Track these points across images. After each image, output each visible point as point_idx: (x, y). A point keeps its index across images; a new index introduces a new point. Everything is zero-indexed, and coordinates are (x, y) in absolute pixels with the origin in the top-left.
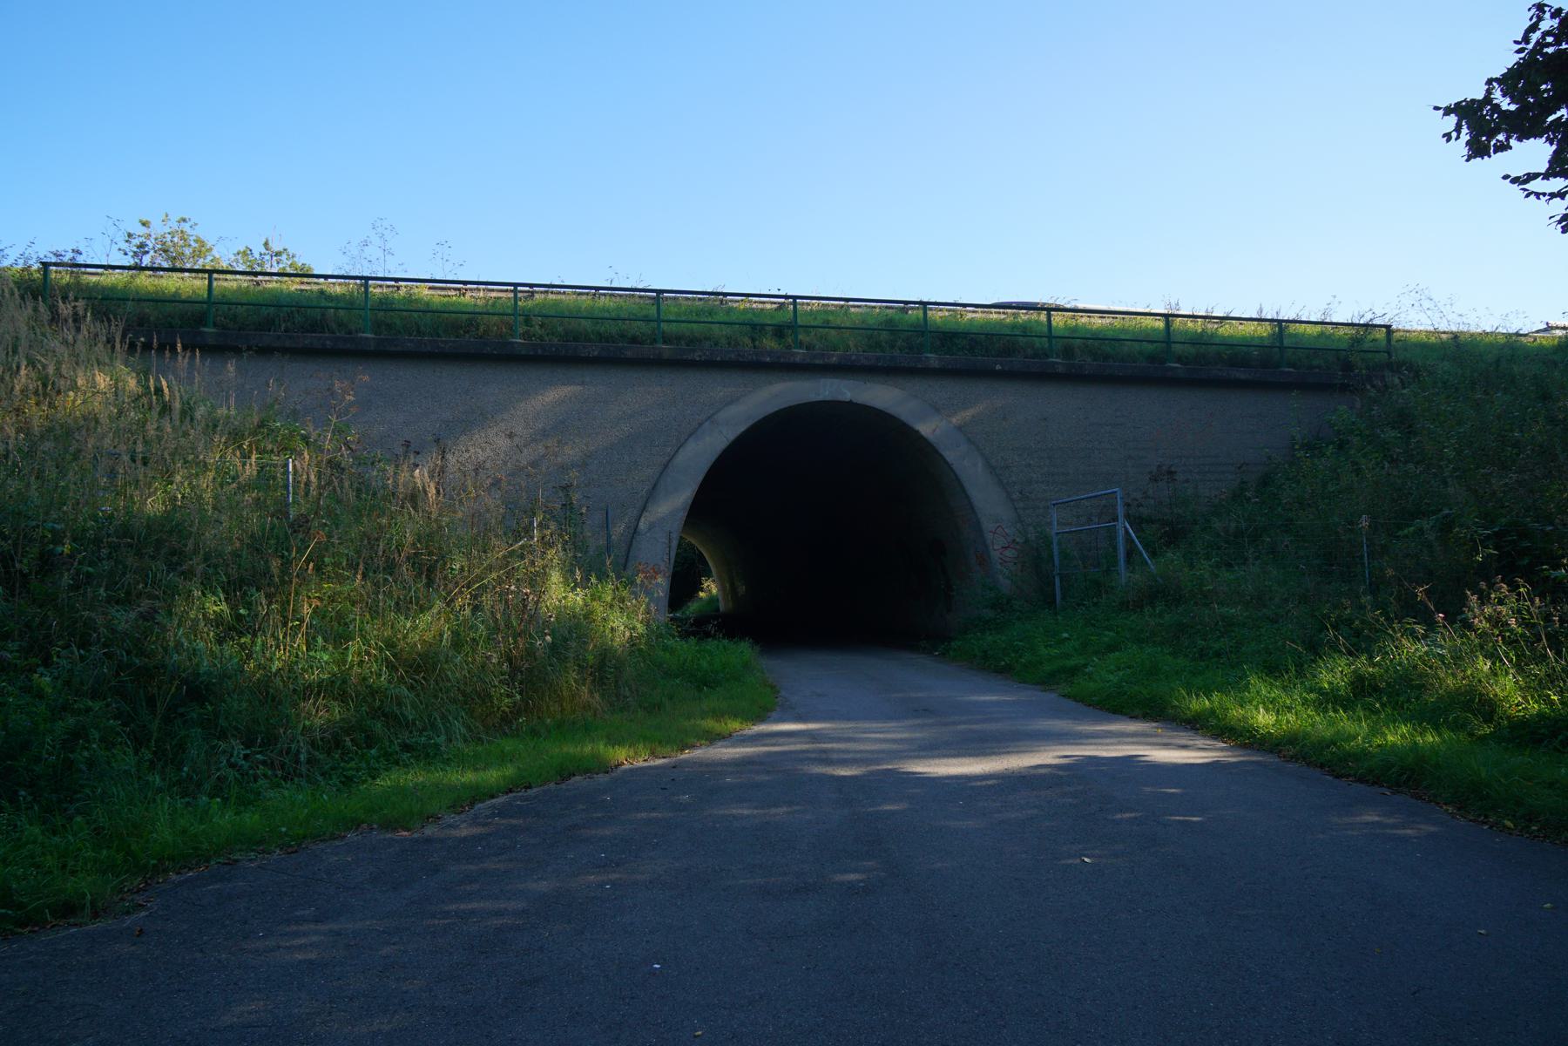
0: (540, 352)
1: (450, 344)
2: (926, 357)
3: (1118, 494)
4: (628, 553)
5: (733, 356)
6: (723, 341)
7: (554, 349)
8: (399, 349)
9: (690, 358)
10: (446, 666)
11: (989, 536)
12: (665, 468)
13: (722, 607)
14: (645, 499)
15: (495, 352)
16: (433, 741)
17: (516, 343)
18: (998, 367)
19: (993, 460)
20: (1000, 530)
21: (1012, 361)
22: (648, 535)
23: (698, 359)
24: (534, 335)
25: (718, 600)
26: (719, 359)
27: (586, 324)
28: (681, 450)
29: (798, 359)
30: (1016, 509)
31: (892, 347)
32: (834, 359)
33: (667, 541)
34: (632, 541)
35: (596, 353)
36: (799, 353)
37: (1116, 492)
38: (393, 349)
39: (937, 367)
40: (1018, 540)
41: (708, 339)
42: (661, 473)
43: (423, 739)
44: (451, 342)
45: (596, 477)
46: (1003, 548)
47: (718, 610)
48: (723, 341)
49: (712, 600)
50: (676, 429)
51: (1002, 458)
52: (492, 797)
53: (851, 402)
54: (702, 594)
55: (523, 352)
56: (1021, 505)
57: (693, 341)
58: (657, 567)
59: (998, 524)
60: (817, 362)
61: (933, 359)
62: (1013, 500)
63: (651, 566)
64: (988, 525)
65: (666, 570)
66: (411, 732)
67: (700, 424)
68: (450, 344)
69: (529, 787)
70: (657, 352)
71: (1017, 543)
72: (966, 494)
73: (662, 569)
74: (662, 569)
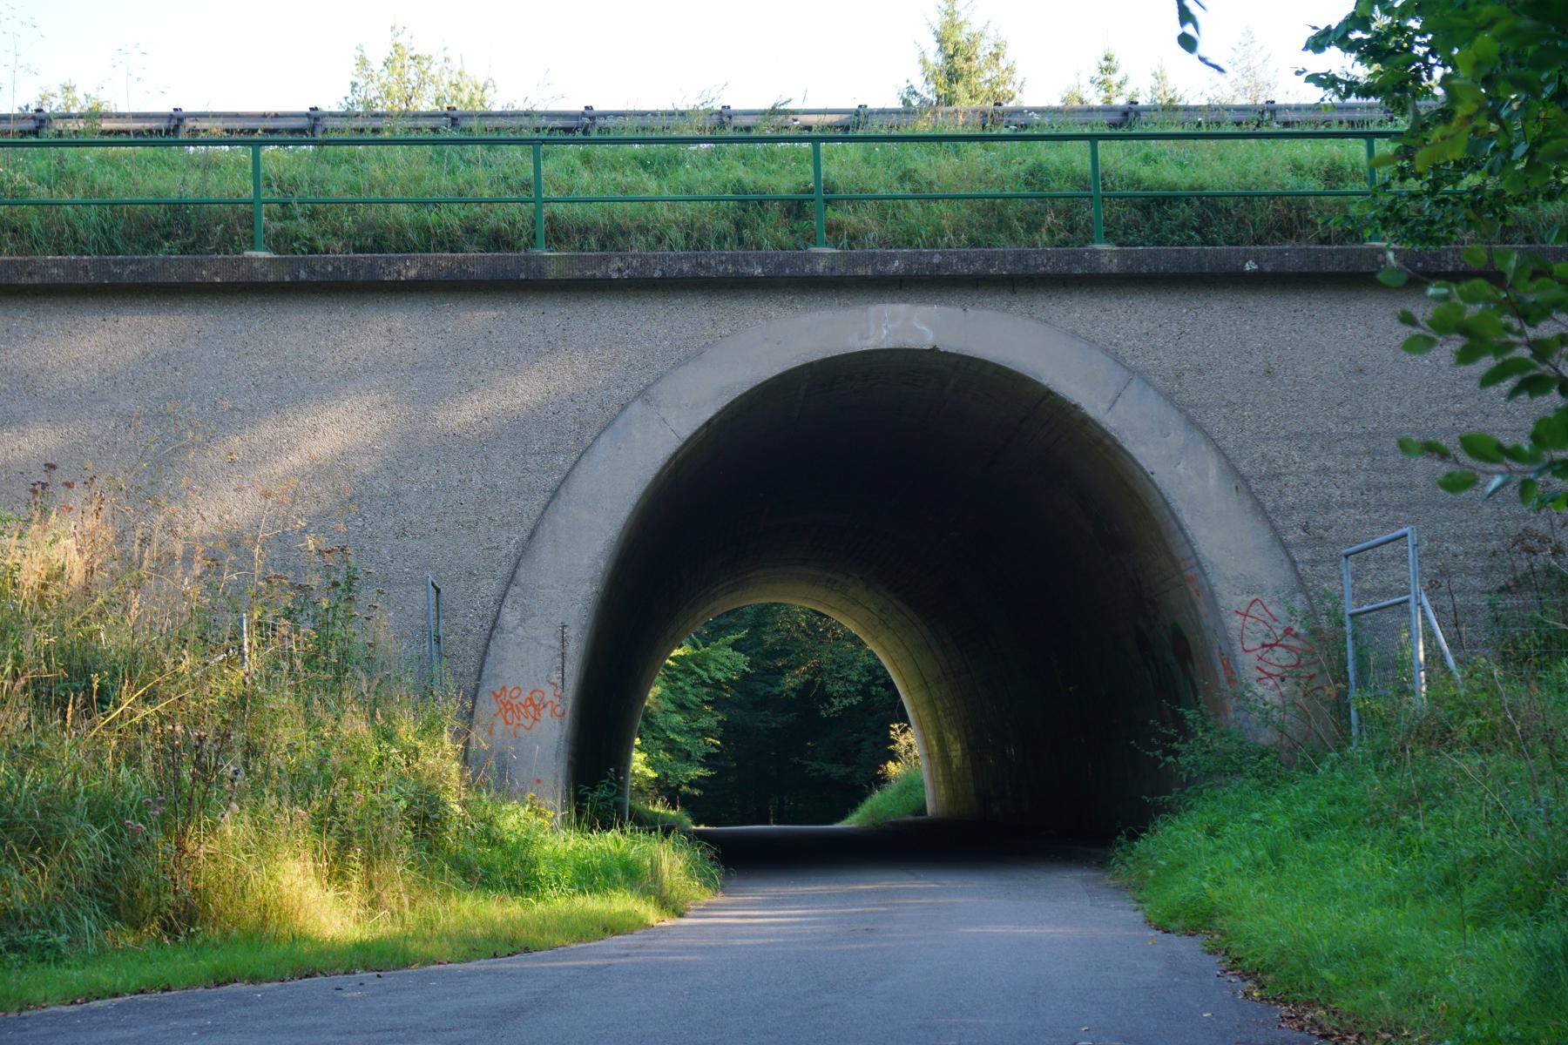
0: (303, 275)
1: (133, 267)
2: (1097, 252)
3: (1409, 538)
4: (481, 670)
5: (686, 267)
6: (674, 233)
7: (330, 269)
8: (37, 280)
9: (598, 275)
10: (76, 843)
11: (1235, 622)
12: (553, 497)
13: (930, 808)
14: (514, 560)
15: (218, 280)
16: (51, 940)
17: (258, 259)
18: (1250, 266)
19: (1245, 462)
20: (1256, 610)
21: (1280, 252)
22: (520, 630)
23: (615, 276)
24: (297, 238)
25: (922, 786)
26: (657, 274)
27: (404, 213)
28: (584, 459)
29: (820, 267)
30: (1294, 563)
31: (1032, 227)
32: (897, 264)
33: (558, 644)
34: (487, 646)
35: (412, 273)
36: (823, 255)
37: (1405, 536)
38: (24, 280)
39: (1115, 269)
40: (1296, 628)
41: (642, 229)
42: (546, 508)
43: (37, 937)
44: (132, 262)
45: (415, 518)
46: (1264, 646)
47: (922, 810)
48: (674, 233)
49: (911, 786)
50: (575, 419)
51: (1264, 456)
52: (116, 995)
53: (934, 350)
54: (892, 768)
55: (271, 278)
56: (1307, 555)
57: (612, 237)
58: (537, 694)
59: (1254, 597)
60: (860, 271)
61: (1106, 254)
62: (1286, 547)
63: (527, 694)
64: (1230, 599)
65: (557, 701)
66: (21, 928)
67: (623, 408)
68: (133, 267)
69: (168, 989)
70: (533, 265)
71: (1296, 636)
72: (1185, 535)
73: (547, 699)
74: (547, 699)
